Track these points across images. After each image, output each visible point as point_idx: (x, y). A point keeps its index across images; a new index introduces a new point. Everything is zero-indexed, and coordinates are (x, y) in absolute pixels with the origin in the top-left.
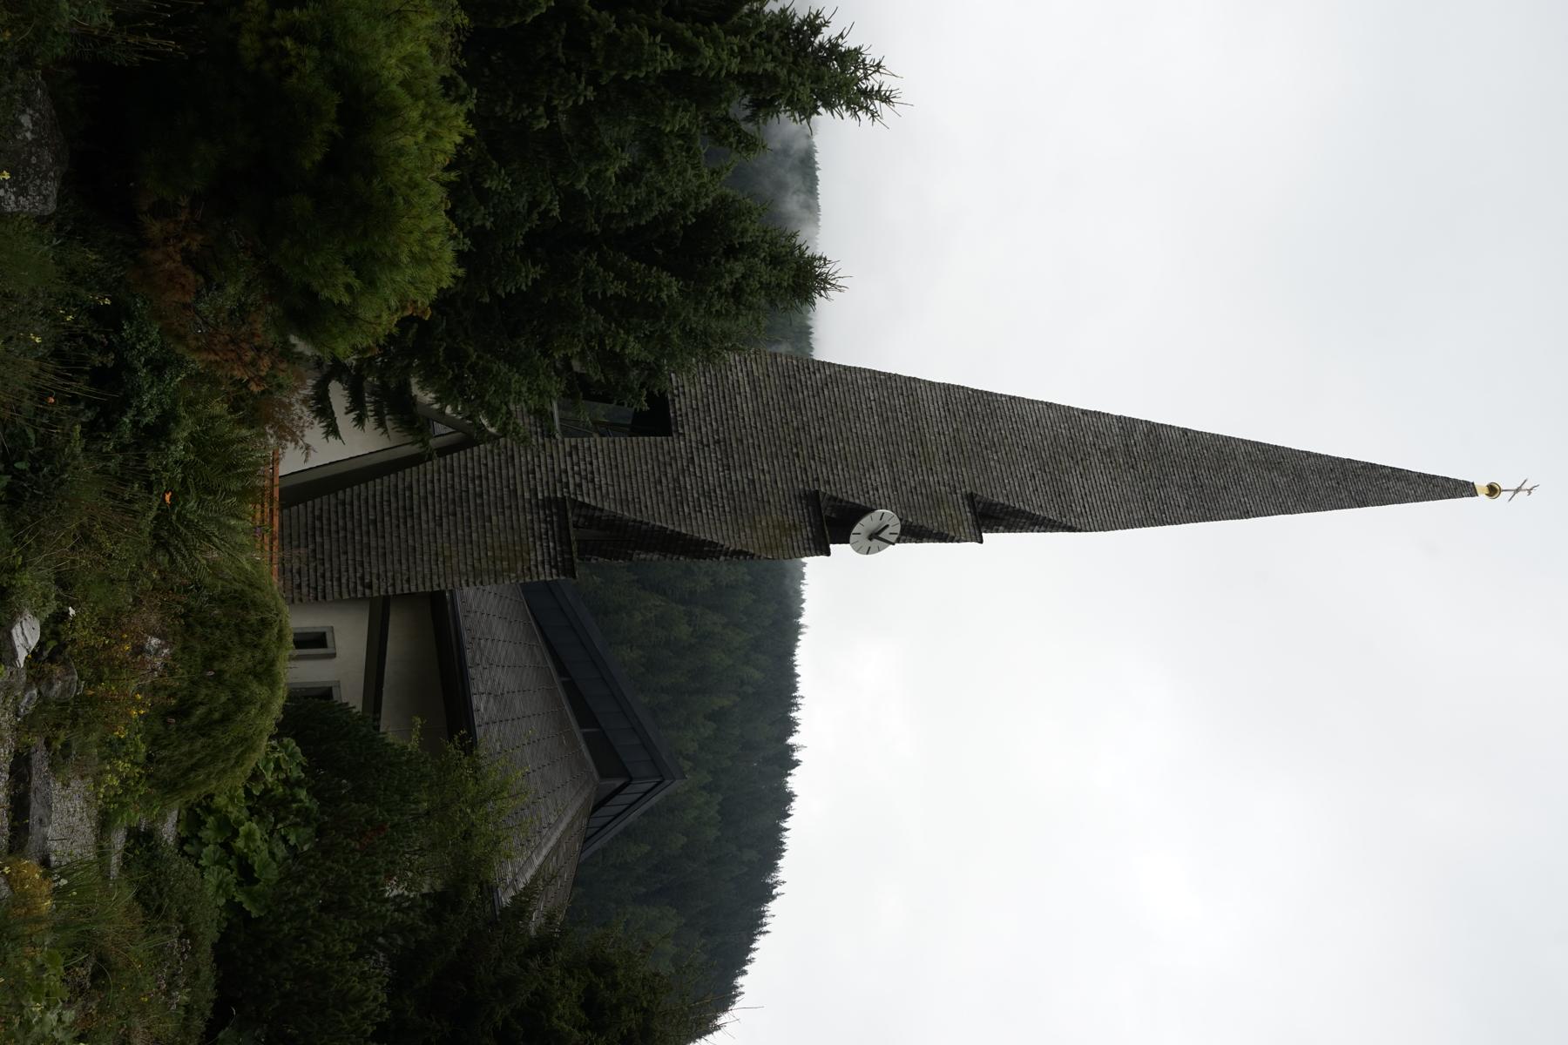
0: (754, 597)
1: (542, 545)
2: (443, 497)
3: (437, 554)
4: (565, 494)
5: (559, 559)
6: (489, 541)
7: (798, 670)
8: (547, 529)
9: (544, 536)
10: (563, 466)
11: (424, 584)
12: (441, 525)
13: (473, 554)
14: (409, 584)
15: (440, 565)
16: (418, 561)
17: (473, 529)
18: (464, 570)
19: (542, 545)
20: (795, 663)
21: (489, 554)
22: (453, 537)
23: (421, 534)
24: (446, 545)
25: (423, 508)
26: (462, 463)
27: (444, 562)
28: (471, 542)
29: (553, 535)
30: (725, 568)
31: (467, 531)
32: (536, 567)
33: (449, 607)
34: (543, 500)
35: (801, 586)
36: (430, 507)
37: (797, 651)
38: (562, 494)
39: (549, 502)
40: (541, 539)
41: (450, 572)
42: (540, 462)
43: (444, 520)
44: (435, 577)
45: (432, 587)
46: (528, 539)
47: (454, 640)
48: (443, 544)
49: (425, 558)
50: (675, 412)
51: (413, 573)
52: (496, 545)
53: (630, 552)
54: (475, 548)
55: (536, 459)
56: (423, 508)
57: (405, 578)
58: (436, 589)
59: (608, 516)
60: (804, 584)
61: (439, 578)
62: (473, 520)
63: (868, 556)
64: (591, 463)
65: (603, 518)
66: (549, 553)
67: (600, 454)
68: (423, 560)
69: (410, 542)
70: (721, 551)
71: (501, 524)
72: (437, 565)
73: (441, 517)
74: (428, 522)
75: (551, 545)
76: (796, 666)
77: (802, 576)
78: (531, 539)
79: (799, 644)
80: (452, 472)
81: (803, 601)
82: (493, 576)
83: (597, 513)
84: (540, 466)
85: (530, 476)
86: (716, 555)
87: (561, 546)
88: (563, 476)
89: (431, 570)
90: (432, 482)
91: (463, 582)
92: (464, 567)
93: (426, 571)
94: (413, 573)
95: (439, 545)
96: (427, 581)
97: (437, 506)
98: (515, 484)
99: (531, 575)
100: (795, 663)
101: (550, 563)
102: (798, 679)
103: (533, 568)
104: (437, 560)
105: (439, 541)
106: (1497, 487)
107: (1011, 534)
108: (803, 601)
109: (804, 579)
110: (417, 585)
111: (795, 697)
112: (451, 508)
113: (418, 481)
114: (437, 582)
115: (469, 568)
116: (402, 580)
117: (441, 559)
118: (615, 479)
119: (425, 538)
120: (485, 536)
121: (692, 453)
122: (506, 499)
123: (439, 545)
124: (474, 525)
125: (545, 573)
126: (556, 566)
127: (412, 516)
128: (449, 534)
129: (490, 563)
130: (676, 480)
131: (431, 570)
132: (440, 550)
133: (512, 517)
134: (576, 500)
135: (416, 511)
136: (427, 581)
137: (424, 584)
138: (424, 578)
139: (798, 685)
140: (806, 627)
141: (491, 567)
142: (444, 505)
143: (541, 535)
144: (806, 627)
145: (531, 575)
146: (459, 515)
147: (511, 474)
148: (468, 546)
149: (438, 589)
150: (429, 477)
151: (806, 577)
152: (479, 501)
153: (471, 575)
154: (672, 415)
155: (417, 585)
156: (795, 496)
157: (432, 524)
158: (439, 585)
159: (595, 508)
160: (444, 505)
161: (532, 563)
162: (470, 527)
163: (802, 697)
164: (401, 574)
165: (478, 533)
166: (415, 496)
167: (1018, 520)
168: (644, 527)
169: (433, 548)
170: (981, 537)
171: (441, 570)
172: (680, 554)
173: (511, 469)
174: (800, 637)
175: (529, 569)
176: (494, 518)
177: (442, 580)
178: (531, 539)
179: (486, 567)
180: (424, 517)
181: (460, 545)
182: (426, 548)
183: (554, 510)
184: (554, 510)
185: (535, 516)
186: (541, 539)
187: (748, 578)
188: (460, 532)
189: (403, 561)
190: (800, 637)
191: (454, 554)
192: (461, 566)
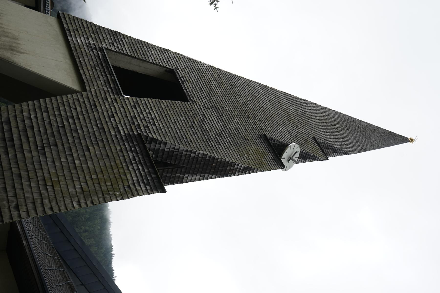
0: (97, 248)
1: (133, 168)
2: (42, 131)
3: (44, 179)
4: (139, 132)
5: (149, 178)
6: (91, 166)
7: (113, 269)
8: (134, 156)
9: (133, 162)
10: (132, 114)
11: (35, 209)
12: (45, 154)
13: (79, 178)
14: (19, 211)
15: (50, 189)
16: (26, 188)
17: (75, 157)
18: (74, 193)
19: (133, 168)
20: (112, 266)
21: (94, 177)
22: (57, 164)
23: (25, 162)
24: (52, 171)
25: (24, 139)
26: (55, 106)
27: (53, 187)
28: (75, 168)
29: (140, 161)
30: (87, 240)
31: (70, 159)
32: (134, 185)
33: (27, 250)
34: (125, 135)
35: (111, 242)
36: (31, 139)
37: (113, 262)
38: (138, 132)
39: (130, 138)
40: (132, 164)
41: (61, 195)
42: (116, 110)
43: (47, 150)
44: (46, 202)
45: (44, 211)
46: (122, 164)
47: (35, 272)
48: (49, 170)
49: (33, 184)
50: (186, 90)
51: (21, 200)
52: (98, 169)
53: (181, 176)
54: (80, 173)
55: (113, 108)
56: (24, 139)
57: (13, 205)
58: (49, 212)
59: (169, 148)
60: (112, 241)
61: (50, 203)
62: (74, 150)
63: (286, 171)
64: (150, 113)
65: (166, 150)
66: (141, 175)
67: (153, 108)
68: (30, 186)
69: (14, 169)
70: (237, 168)
71: (98, 152)
72: (47, 189)
73: (43, 148)
74: (30, 152)
75: (140, 167)
76: (113, 267)
77: (111, 238)
78: (124, 164)
79: (113, 260)
80: (47, 112)
81: (112, 246)
82: (101, 196)
83: (162, 146)
84: (116, 113)
85: (111, 119)
86: (234, 172)
87: (148, 169)
88: (135, 120)
89: (41, 195)
90: (30, 118)
91: (75, 203)
92: (73, 189)
93: (36, 196)
94: (21, 200)
95: (46, 172)
96: (38, 205)
97: (38, 138)
98: (102, 124)
99: (132, 192)
100: (112, 266)
101: (143, 182)
102: (114, 272)
103: (132, 186)
104: (46, 185)
105: (45, 167)
106: (413, 139)
107: (307, 163)
108: (112, 246)
109: (112, 239)
110: (27, 211)
111: (114, 277)
112: (51, 140)
113: (15, 117)
114: (49, 207)
115: (78, 190)
116: (9, 208)
117: (49, 184)
118: (168, 124)
119: (30, 166)
120: (87, 163)
121: (203, 112)
122: (97, 134)
123: (46, 172)
124: (75, 154)
125: (142, 189)
126: (149, 184)
127: (13, 146)
128: (53, 162)
129: (96, 185)
130: (201, 126)
131: (41, 195)
132: (47, 176)
133: (105, 147)
134: (148, 136)
135: (16, 142)
136: (38, 205)
137: (35, 209)
138: (34, 203)
139: (114, 273)
140: (114, 254)
141: (98, 188)
142: (44, 137)
143: (131, 162)
144: (114, 254)
145: (132, 192)
146: (60, 145)
147: (97, 116)
148: (73, 172)
149: (52, 213)
150: (26, 114)
151: (112, 239)
152: (75, 135)
153: (82, 196)
154: (185, 91)
155: (27, 211)
156: (257, 137)
157: (35, 154)
158: (51, 209)
159: (160, 143)
160: (44, 137)
161: (130, 182)
162: (72, 155)
163: (116, 277)
164: (8, 201)
165: (80, 160)
166: (14, 130)
167: (329, 151)
168: (193, 155)
169: (39, 174)
170: (328, 159)
171: (51, 194)
172: (213, 174)
173: (95, 113)
174: (113, 258)
175: (129, 187)
176: (91, 148)
177: (54, 204)
178: (124, 164)
179: (93, 188)
180: (26, 147)
181: (66, 171)
182: (32, 175)
183: (135, 143)
184: (135, 143)
185: (123, 147)
186: (132, 164)
187: (94, 242)
188: (63, 160)
189: (9, 188)
190: (113, 258)
191: (61, 178)
192: (71, 189)
